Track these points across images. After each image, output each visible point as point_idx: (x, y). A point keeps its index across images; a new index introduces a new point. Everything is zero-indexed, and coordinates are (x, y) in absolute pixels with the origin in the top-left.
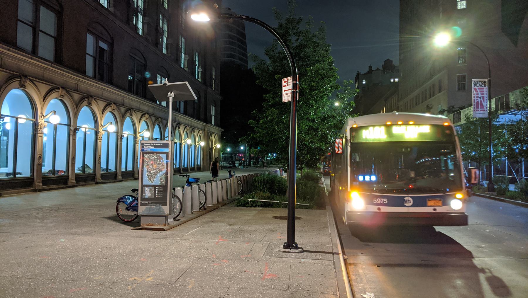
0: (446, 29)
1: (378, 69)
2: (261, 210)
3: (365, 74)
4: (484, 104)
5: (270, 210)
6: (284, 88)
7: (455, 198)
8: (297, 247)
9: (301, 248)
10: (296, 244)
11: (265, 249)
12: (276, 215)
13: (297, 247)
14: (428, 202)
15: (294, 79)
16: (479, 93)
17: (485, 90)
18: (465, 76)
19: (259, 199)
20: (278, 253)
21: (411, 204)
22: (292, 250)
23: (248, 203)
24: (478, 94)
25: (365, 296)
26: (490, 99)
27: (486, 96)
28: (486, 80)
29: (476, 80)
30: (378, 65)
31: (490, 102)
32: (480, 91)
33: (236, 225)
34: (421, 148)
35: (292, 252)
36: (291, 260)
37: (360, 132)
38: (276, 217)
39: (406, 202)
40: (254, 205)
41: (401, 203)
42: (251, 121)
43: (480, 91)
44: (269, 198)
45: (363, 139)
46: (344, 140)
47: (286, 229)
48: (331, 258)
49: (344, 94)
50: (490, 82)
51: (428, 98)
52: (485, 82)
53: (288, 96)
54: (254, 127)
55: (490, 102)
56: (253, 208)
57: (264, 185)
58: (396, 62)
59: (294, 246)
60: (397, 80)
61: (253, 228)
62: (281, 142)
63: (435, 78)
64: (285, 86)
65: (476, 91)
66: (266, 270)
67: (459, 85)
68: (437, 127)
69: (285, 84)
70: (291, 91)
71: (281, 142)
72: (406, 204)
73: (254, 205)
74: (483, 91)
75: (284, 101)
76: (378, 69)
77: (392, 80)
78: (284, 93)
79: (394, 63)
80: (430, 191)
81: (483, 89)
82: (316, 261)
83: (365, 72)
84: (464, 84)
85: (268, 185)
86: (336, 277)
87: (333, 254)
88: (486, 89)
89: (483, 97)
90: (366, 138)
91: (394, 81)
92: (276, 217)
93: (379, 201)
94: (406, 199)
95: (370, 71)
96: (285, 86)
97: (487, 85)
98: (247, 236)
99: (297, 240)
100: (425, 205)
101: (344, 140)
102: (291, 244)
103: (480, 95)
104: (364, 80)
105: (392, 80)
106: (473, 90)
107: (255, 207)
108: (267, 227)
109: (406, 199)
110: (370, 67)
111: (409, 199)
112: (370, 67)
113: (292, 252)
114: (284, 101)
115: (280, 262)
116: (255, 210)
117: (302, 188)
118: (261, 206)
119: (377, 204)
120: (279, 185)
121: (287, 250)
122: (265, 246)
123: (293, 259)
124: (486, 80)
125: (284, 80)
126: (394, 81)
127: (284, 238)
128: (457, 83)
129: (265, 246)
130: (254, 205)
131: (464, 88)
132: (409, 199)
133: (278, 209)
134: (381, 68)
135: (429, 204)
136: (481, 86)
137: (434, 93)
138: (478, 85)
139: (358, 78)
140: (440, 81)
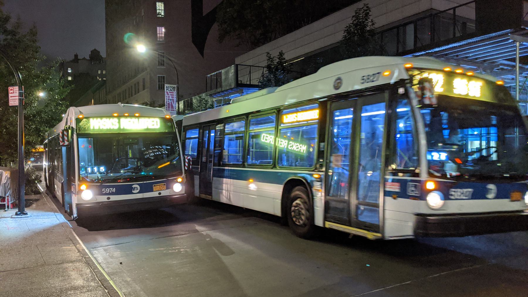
0: (129, 47)
3: (72, 61)
4: (174, 105)
6: (10, 95)
7: (177, 182)
14: (154, 187)
21: (138, 191)
26: (178, 101)
27: (175, 99)
29: (168, 85)
31: (179, 104)
34: (149, 139)
37: (456, 77)
39: (134, 189)
41: (129, 190)
45: (90, 130)
46: (70, 131)
51: (133, 94)
52: (174, 88)
55: (179, 104)
58: (103, 54)
63: (139, 76)
65: (168, 94)
67: (159, 84)
68: (165, 120)
70: (17, 98)
72: (134, 192)
75: (10, 105)
76: (84, 59)
78: (10, 98)
79: (101, 54)
80: (156, 177)
88: (175, 93)
89: (173, 100)
90: (94, 129)
93: (108, 190)
94: (133, 186)
95: (76, 59)
100: (152, 190)
101: (70, 131)
103: (171, 98)
104: (69, 69)
106: (166, 93)
109: (133, 186)
110: (76, 56)
111: (136, 186)
112: (76, 56)
114: (10, 105)
119: (106, 194)
124: (175, 86)
125: (10, 88)
132: (136, 186)
134: (88, 58)
135: (154, 190)
139: (63, 66)
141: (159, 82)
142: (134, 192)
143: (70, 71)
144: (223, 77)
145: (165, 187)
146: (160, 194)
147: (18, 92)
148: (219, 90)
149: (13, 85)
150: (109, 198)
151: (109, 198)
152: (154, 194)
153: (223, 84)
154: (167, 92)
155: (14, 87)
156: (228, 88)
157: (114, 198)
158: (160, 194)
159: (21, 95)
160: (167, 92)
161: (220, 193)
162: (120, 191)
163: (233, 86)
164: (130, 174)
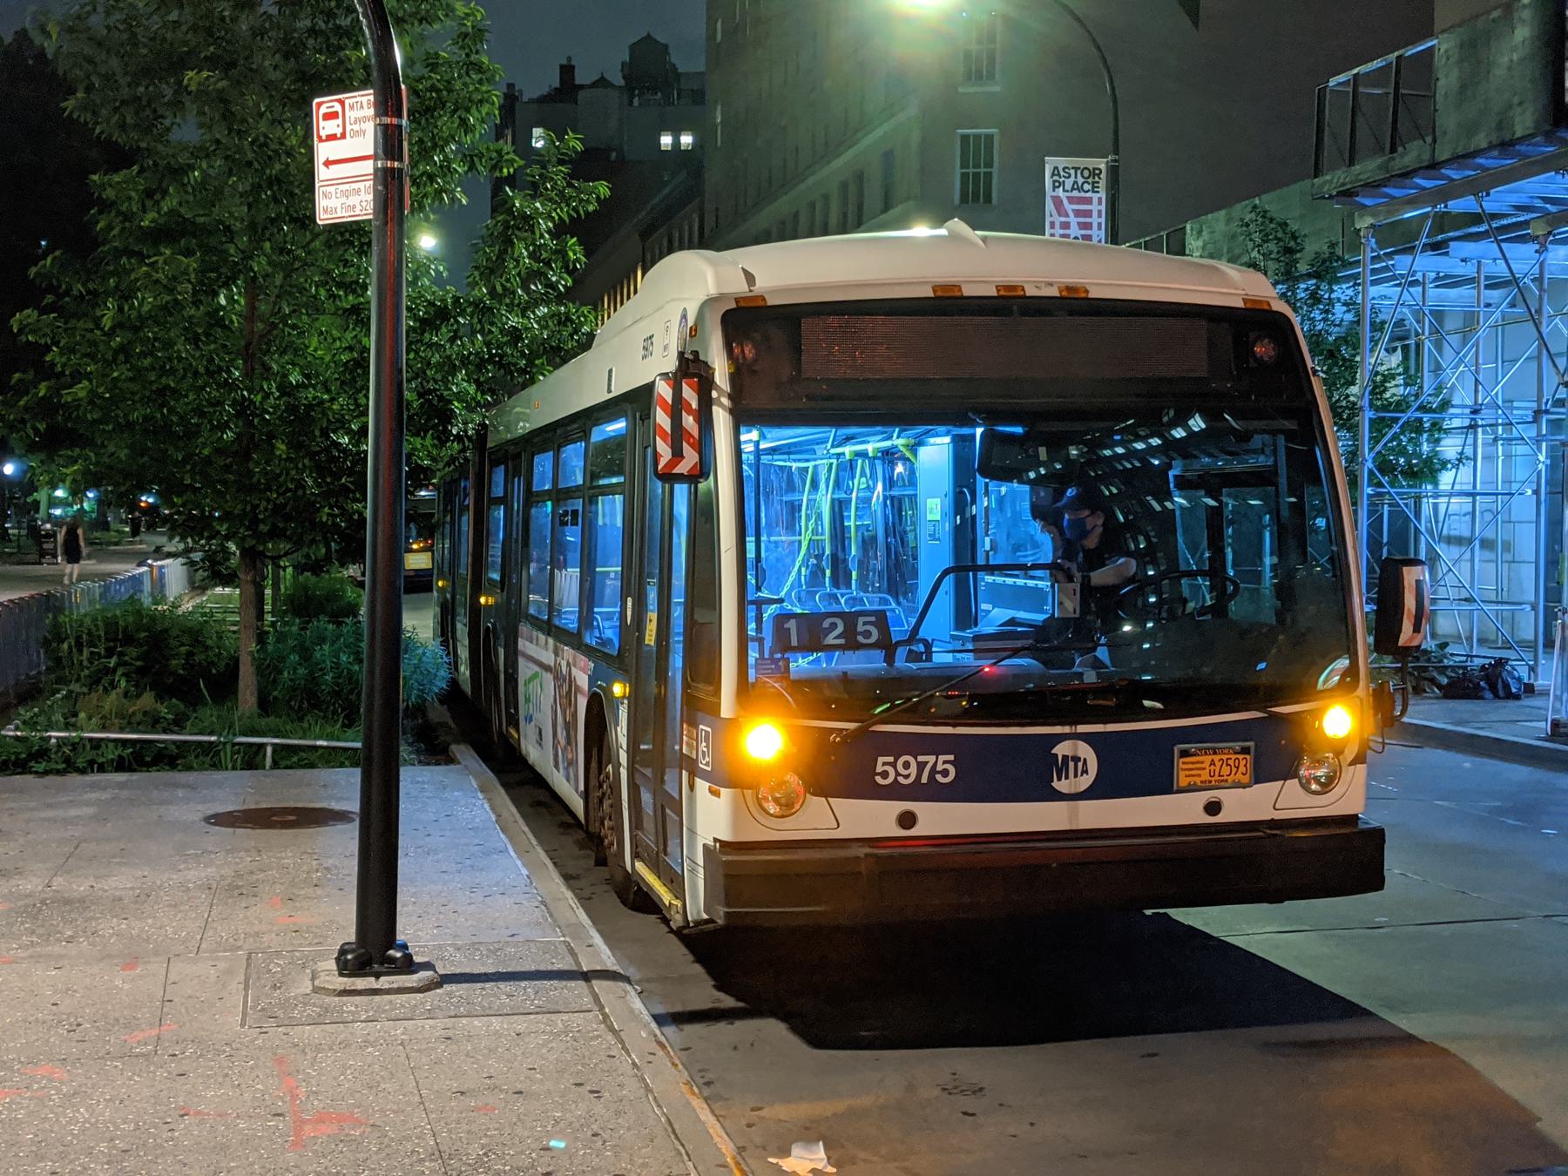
1: (602, 82)
2: (122, 786)
3: (542, 100)
5: (177, 785)
6: (323, 151)
8: (408, 965)
9: (428, 966)
10: (404, 947)
11: (236, 985)
12: (221, 809)
13: (408, 965)
14: (1181, 764)
15: (387, 104)
16: (1073, 220)
17: (1094, 207)
18: (989, 138)
19: (104, 728)
20: (316, 999)
21: (1085, 782)
22: (385, 982)
23: (42, 753)
24: (1066, 226)
25: (787, 1164)
28: (1102, 164)
29: (1061, 162)
30: (604, 60)
32: (1078, 213)
33: (18, 871)
35: (388, 992)
36: (399, 1030)
38: (220, 820)
39: (1063, 767)
40: (80, 762)
41: (1031, 776)
42: (30, 315)
43: (1078, 213)
44: (155, 723)
47: (355, 883)
48: (587, 1001)
49: (534, 197)
50: (1114, 171)
52: (1095, 173)
53: (346, 194)
54: (48, 349)
56: (75, 779)
57: (110, 653)
59: (393, 960)
60: (687, 140)
61: (121, 881)
62: (213, 429)
63: (867, 141)
64: (332, 137)
66: (294, 1097)
67: (964, 176)
69: (328, 127)
70: (368, 167)
71: (213, 429)
72: (1061, 785)
73: (78, 761)
74: (1088, 214)
75: (323, 218)
76: (602, 82)
77: (666, 140)
78: (322, 173)
81: (1089, 201)
82: (521, 1024)
83: (545, 90)
84: (989, 176)
85: (133, 652)
86: (648, 1090)
87: (587, 976)
91: (676, 142)
92: (220, 820)
93: (907, 769)
94: (1061, 750)
95: (568, 87)
96: (332, 137)
97: (1102, 184)
98: (109, 926)
99: (405, 930)
100: (1163, 784)
102: (375, 950)
104: (537, 132)
105: (666, 140)
106: (1049, 206)
107: (82, 772)
108: (195, 874)
110: (567, 70)
111: (1077, 749)
112: (567, 70)
113: (388, 992)
114: (323, 218)
115: (345, 1045)
116: (93, 787)
117: (338, 665)
118: (121, 766)
120: (190, 654)
121: (361, 983)
122: (230, 972)
123: (390, 1018)
124: (1102, 164)
125: (324, 104)
126: (676, 142)
127: (341, 920)
128: (958, 171)
129: (230, 972)
130: (80, 762)
131: (988, 199)
132: (1077, 749)
133: (218, 776)
134: (619, 80)
135: (1183, 781)
136: (1080, 189)
137: (860, 207)
138: (1069, 184)
140: (888, 156)
141: (964, 165)
142: (1061, 785)
143: (539, 144)
144: (1447, 81)
145: (1245, 761)
146: (1213, 808)
147: (370, 127)
148: (1413, 153)
149: (340, 83)
150: (907, 820)
151: (907, 820)
152: (1175, 810)
153: (1448, 120)
154: (1058, 202)
155: (351, 98)
156: (1481, 141)
157: (941, 819)
158: (1213, 808)
159: (389, 142)
160: (1058, 202)
161: (415, 608)
162: (984, 777)
163: (1524, 121)
164: (968, 659)
